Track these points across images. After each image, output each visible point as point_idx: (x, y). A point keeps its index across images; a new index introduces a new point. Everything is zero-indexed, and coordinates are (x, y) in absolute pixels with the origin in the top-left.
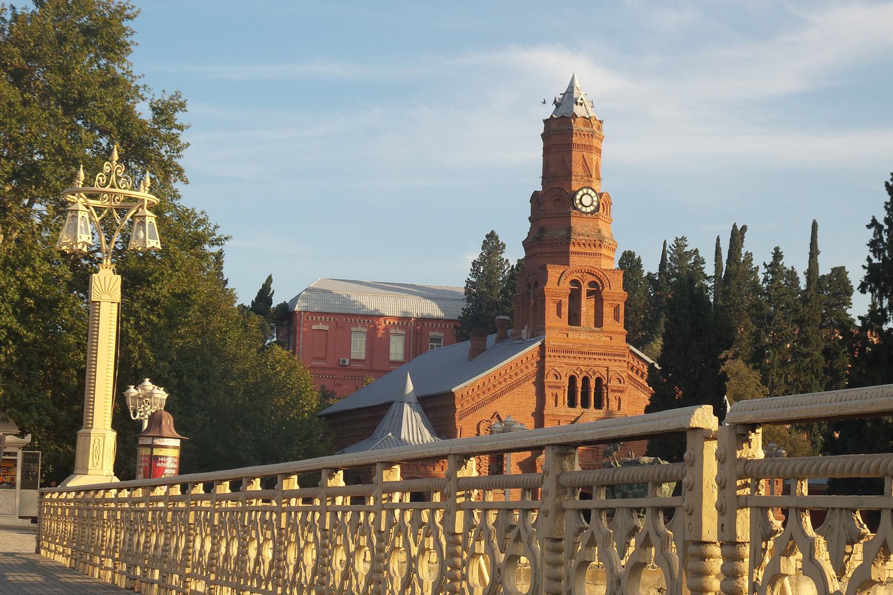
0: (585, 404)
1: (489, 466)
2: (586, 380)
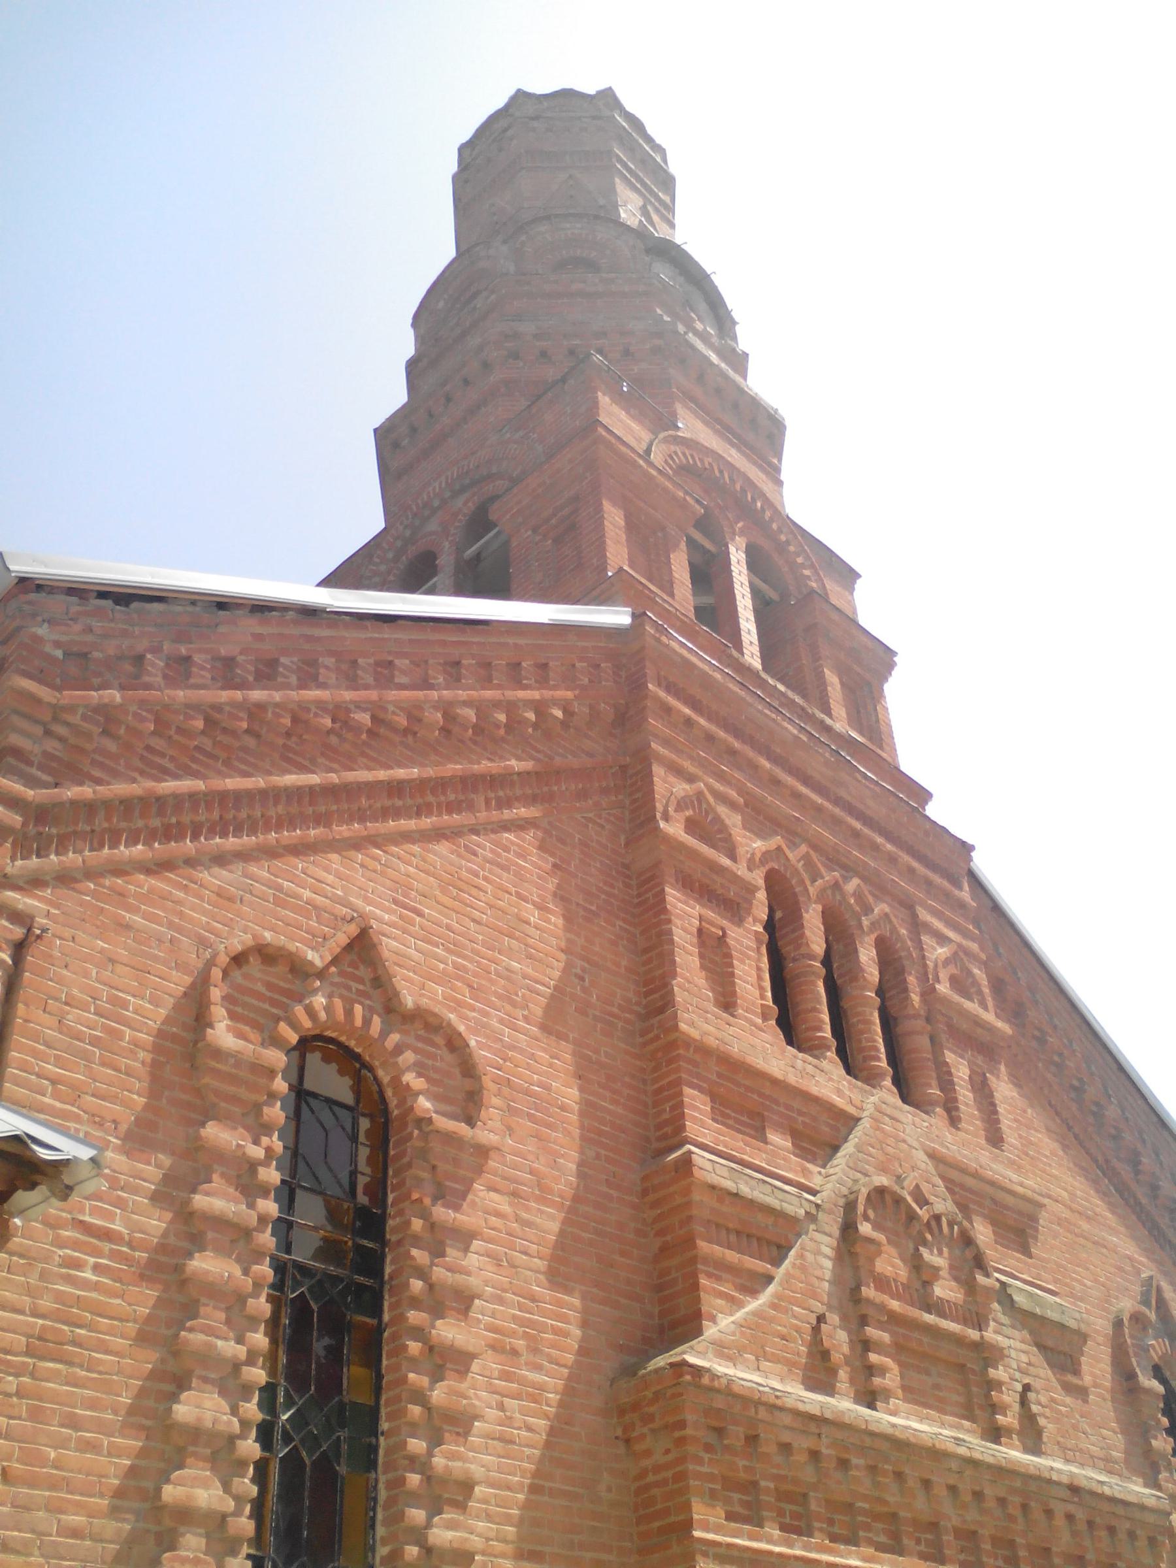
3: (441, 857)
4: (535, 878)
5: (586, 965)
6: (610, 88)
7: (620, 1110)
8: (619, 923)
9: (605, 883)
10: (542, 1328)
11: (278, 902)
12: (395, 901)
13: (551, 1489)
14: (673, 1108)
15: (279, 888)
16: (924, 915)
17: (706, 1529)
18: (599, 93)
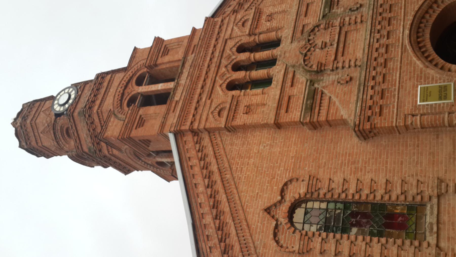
0: (271, 62)
2: (237, 67)
4: (242, 160)
5: (261, 145)
6: (11, 124)
7: (295, 135)
8: (249, 135)
9: (239, 139)
10: (349, 160)
12: (256, 200)
15: (259, 232)
16: (227, 36)
17: (392, 122)
18: (14, 127)
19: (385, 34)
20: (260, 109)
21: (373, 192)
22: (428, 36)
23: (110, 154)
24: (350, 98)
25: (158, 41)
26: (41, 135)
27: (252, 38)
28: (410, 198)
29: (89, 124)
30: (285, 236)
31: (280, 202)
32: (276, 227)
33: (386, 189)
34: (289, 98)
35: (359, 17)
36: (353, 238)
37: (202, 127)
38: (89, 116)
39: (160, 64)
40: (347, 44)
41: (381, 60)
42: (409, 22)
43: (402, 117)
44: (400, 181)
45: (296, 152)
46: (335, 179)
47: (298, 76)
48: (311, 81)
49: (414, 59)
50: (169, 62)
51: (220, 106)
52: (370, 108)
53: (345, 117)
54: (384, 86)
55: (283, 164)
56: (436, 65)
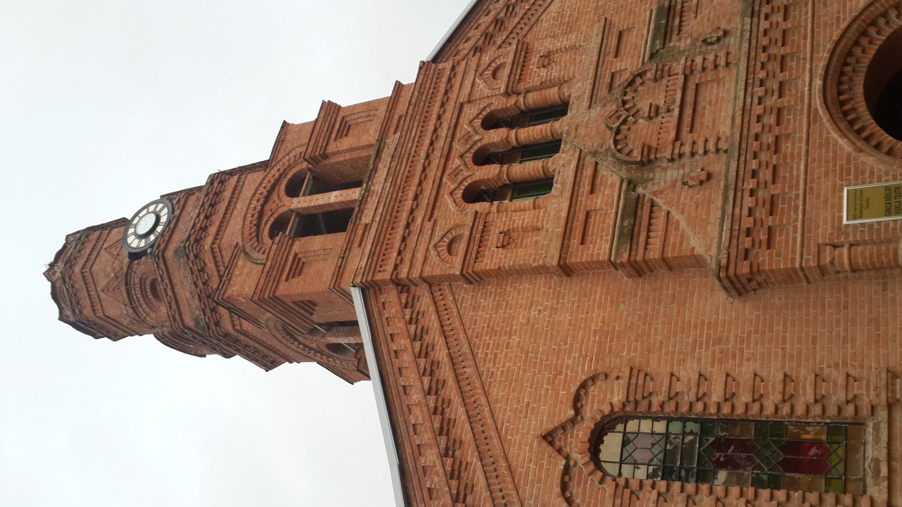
0: (551, 147)
1: (758, 483)
2: (483, 157)
3: (498, 392)
9: (490, 297)
11: (539, 481)
13: (783, 332)
14: (594, 264)
15: (533, 481)
17: (793, 260)
19: (776, 87)
20: (530, 239)
21: (758, 398)
22: (859, 90)
23: (237, 331)
24: (708, 213)
25: (329, 109)
26: (103, 295)
27: (512, 101)
28: (832, 411)
29: (196, 273)
30: (585, 489)
31: (573, 421)
32: (567, 470)
33: (784, 393)
34: (588, 215)
35: (722, 55)
36: (719, 490)
37: (415, 274)
38: (196, 257)
39: (334, 154)
40: (699, 109)
41: (769, 139)
42: (822, 64)
43: (814, 249)
44: (811, 377)
45: (603, 322)
46: (683, 374)
47: (603, 171)
48: (629, 182)
49: (834, 135)
50: (351, 150)
51: (451, 234)
52: (748, 233)
53: (700, 250)
54: (775, 190)
55: (577, 345)
56: (878, 147)
